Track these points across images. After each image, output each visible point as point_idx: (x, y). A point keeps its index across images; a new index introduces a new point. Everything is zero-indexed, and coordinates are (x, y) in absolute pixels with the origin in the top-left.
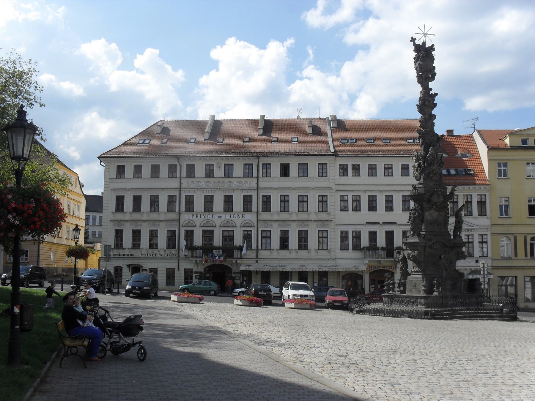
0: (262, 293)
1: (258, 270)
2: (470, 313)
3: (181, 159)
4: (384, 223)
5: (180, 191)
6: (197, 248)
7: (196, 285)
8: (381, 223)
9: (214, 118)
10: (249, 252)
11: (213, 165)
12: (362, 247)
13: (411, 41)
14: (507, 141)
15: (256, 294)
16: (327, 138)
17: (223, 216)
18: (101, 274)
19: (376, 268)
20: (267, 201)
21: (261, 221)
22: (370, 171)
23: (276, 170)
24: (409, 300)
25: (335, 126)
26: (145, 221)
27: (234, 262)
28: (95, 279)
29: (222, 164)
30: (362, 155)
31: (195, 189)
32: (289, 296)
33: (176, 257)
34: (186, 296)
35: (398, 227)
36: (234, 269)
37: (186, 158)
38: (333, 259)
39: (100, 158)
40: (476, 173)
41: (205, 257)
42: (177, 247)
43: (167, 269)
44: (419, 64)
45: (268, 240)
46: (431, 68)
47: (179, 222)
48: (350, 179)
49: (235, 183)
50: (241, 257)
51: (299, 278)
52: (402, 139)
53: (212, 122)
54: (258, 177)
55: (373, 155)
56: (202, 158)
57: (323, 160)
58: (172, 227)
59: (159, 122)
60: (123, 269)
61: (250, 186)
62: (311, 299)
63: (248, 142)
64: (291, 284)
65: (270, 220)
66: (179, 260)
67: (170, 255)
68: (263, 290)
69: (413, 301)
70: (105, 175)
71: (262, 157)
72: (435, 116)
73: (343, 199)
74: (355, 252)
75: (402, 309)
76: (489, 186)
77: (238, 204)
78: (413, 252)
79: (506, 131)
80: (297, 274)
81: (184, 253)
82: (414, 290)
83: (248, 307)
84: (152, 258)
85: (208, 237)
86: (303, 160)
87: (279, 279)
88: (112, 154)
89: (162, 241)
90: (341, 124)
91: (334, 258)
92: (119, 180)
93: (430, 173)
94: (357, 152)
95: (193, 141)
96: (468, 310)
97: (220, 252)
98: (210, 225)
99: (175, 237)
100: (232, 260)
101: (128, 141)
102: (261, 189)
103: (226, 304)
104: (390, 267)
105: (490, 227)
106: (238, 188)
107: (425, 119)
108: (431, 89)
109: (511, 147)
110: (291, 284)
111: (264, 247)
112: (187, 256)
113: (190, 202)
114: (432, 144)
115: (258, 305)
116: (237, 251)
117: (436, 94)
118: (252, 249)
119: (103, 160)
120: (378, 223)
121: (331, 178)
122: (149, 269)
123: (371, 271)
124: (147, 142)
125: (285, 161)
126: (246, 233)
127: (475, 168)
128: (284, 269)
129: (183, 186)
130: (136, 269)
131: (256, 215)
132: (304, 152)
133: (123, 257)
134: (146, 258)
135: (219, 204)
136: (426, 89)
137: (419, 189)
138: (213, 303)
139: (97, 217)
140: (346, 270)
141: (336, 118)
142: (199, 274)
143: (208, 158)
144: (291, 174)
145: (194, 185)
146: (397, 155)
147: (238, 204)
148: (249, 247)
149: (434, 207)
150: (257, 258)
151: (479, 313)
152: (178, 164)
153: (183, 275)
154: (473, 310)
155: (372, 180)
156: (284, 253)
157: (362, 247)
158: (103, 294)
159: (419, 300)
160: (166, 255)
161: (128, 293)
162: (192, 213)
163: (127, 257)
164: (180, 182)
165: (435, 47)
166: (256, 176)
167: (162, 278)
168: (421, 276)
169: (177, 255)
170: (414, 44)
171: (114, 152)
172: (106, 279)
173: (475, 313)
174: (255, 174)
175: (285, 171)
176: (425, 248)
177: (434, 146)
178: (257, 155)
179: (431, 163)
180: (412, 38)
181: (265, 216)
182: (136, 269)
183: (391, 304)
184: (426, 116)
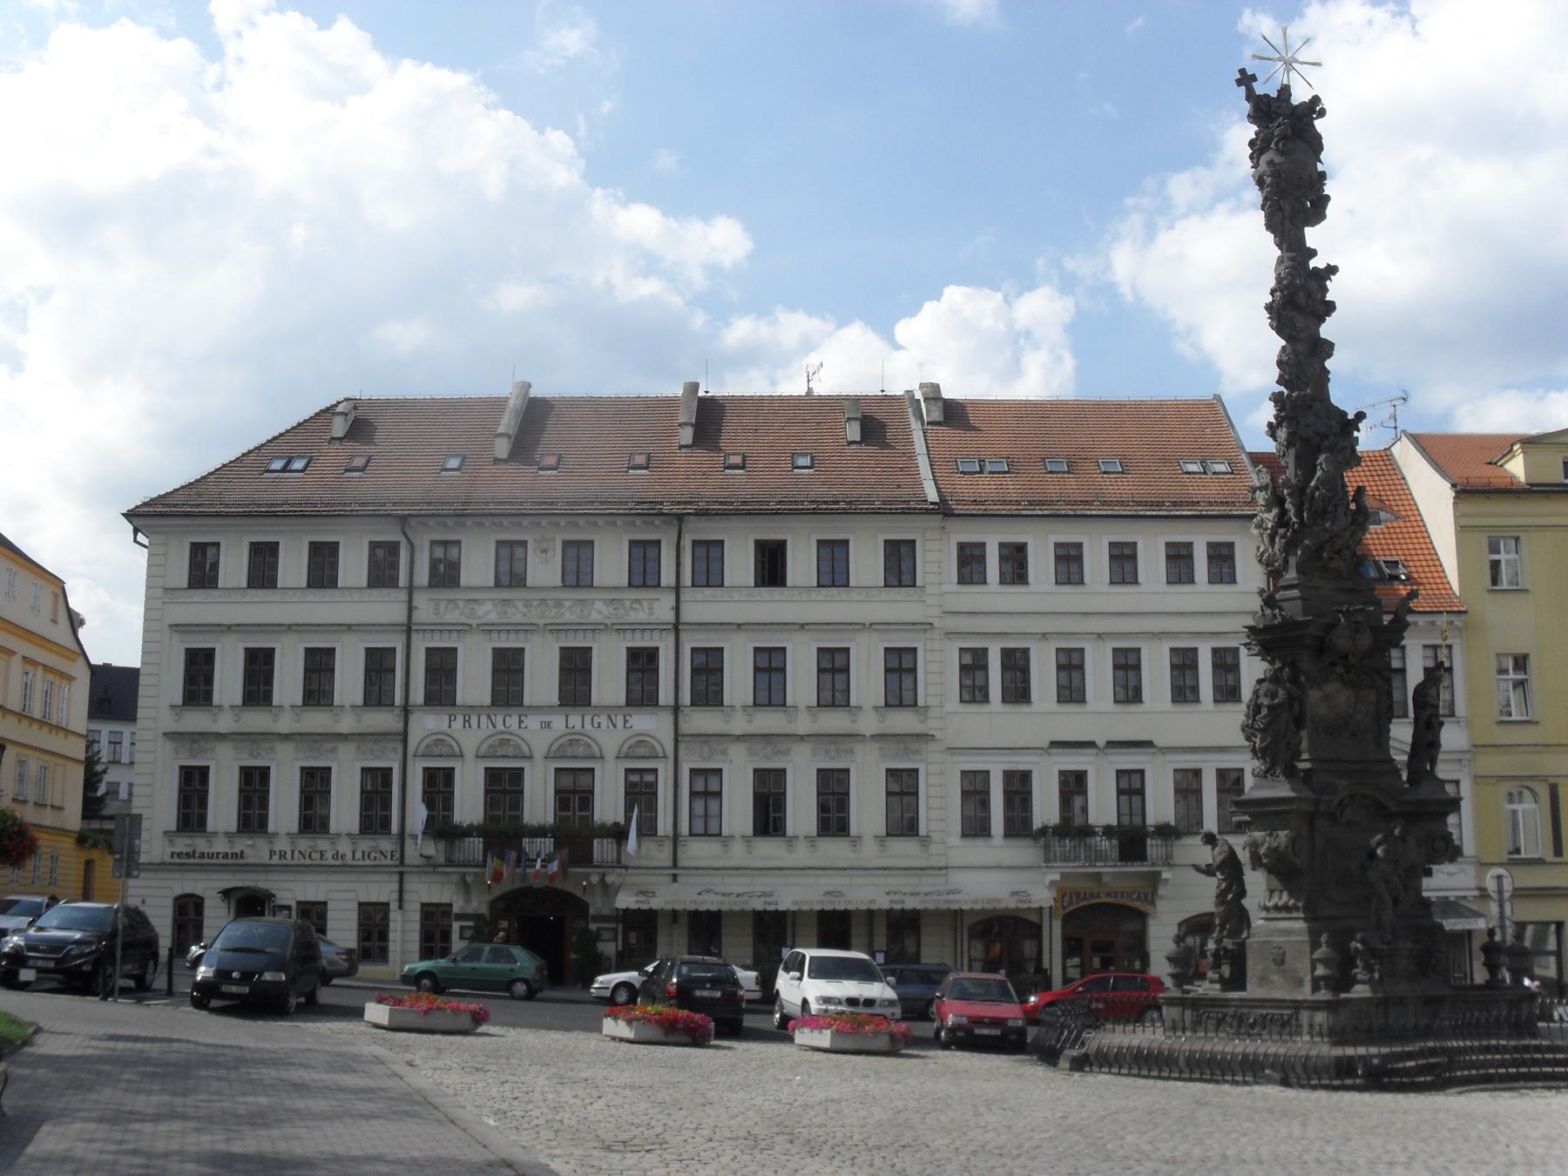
0: (706, 994)
1: (679, 907)
2: (1502, 1064)
3: (413, 522)
4: (1112, 744)
7: (464, 960)
8: (1101, 743)
9: (527, 392)
10: (649, 845)
11: (524, 543)
12: (1037, 823)
13: (1239, 82)
14: (1517, 467)
15: (684, 996)
16: (911, 456)
17: (558, 722)
19: (1085, 898)
20: (708, 668)
22: (1062, 568)
23: (740, 563)
24: (1264, 1017)
25: (937, 419)
26: (286, 737)
27: (595, 879)
28: (78, 942)
29: (554, 540)
30: (1035, 513)
31: (462, 629)
32: (805, 1002)
33: (392, 863)
34: (424, 1005)
35: (1160, 758)
36: (596, 905)
37: (432, 522)
38: (940, 869)
40: (1416, 575)
41: (493, 863)
43: (361, 904)
44: (1271, 163)
45: (713, 804)
46: (1311, 176)
47: (405, 742)
48: (993, 594)
49: (599, 606)
50: (619, 864)
51: (818, 940)
52: (1165, 460)
53: (520, 402)
54: (677, 588)
55: (1072, 513)
57: (900, 530)
59: (339, 403)
60: (207, 903)
61: (652, 619)
62: (888, 1012)
64: (811, 958)
66: (401, 874)
69: (1283, 1019)
71: (692, 517)
72: (1330, 346)
73: (974, 664)
74: (1013, 842)
75: (1239, 1049)
76: (1463, 617)
77: (609, 681)
78: (1271, 835)
79: (1515, 436)
81: (420, 848)
82: (1275, 978)
84: (307, 866)
85: (505, 792)
86: (834, 530)
87: (750, 940)
88: (175, 506)
89: (345, 808)
90: (954, 414)
91: (942, 863)
92: (199, 595)
93: (1320, 548)
95: (806, 461)
96: (1487, 1050)
97: (547, 845)
98: (510, 751)
99: (391, 793)
100: (589, 874)
101: (231, 462)
102: (688, 627)
103: (573, 1035)
104: (1133, 893)
105: (1468, 756)
106: (608, 622)
107: (1296, 357)
108: (1313, 253)
109: (1532, 485)
110: (811, 958)
111: (699, 828)
113: (442, 668)
114: (1326, 443)
115: (696, 1038)
116: (605, 841)
117: (1332, 270)
118: (656, 834)
120: (1091, 744)
121: (930, 589)
122: (299, 903)
123: (1068, 910)
124: (298, 465)
125: (771, 531)
126: (635, 778)
127: (1409, 558)
129: (417, 618)
130: (250, 903)
132: (837, 502)
134: (287, 866)
135: (542, 679)
136: (1295, 252)
137: (1284, 605)
138: (524, 1031)
140: (987, 906)
141: (939, 391)
142: (471, 924)
143: (506, 522)
144: (791, 577)
145: (457, 612)
146: (1154, 513)
147: (609, 681)
148: (648, 829)
149: (1340, 670)
150: (675, 865)
151: (1535, 1063)
153: (416, 926)
154: (1505, 1049)
155: (1069, 598)
156: (769, 850)
157: (1037, 823)
158: (104, 999)
159: (1304, 1016)
160: (359, 855)
161: (205, 997)
163: (221, 861)
164: (410, 601)
165: (1326, 103)
166: (673, 582)
167: (342, 932)
168: (1301, 925)
169: (398, 855)
170: (1251, 95)
171: (179, 499)
173: (1514, 1063)
174: (667, 577)
175: (771, 564)
176: (1312, 818)
177: (1331, 450)
178: (676, 509)
179: (1325, 512)
180: (1242, 71)
181: (701, 721)
182: (250, 903)
183: (1194, 1031)
184: (1300, 347)
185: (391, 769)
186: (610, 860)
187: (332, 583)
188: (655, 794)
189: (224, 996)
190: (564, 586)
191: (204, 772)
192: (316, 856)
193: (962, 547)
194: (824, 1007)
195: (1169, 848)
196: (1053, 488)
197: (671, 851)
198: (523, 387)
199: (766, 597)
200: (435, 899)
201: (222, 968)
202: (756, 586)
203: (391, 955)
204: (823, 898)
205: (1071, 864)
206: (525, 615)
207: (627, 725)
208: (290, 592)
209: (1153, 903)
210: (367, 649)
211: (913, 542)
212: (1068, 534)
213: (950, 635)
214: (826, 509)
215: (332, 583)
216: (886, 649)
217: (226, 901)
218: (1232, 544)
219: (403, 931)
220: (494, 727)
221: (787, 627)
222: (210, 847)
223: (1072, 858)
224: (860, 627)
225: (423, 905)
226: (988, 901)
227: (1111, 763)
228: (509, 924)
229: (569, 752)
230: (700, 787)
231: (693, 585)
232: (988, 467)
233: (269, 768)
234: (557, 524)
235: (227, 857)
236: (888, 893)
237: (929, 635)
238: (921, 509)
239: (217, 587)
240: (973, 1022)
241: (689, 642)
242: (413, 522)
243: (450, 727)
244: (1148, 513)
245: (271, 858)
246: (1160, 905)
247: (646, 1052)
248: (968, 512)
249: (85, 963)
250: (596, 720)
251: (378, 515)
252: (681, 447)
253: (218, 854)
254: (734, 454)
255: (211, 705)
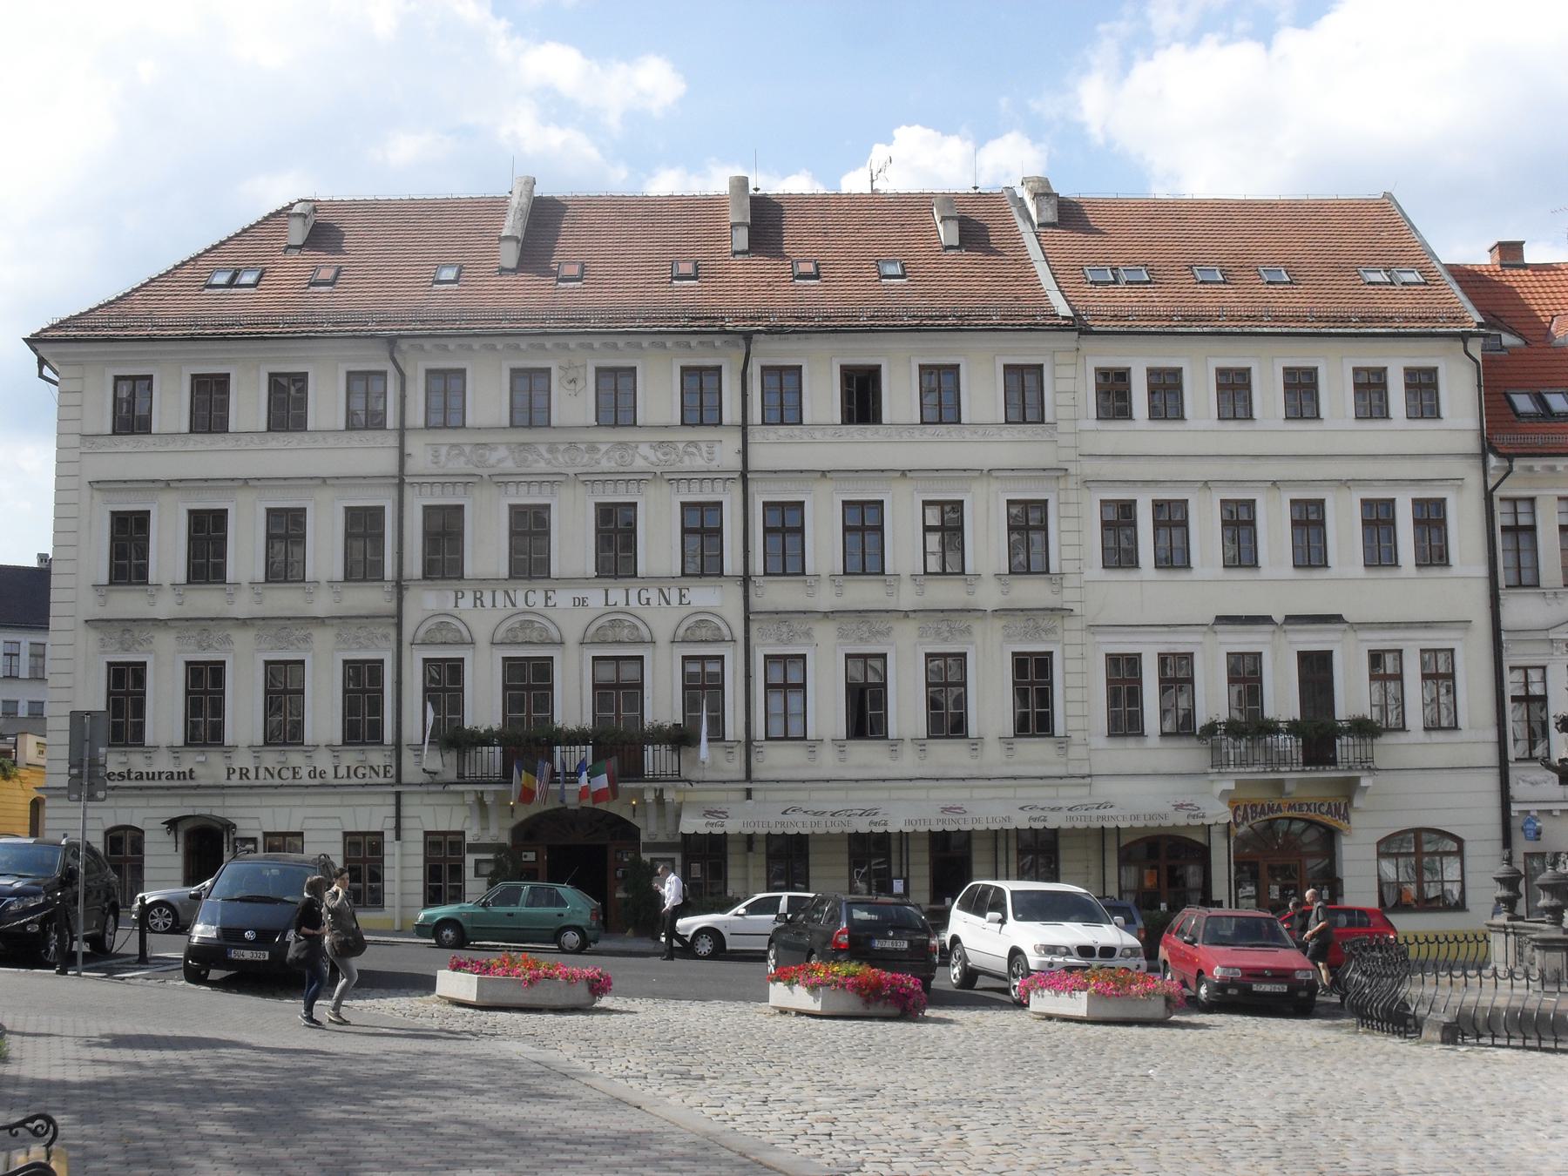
0: (888, 944)
4: (1291, 619)
5: (401, 485)
6: (485, 739)
8: (1278, 617)
12: (1201, 720)
16: (1026, 263)
17: (595, 598)
18: (53, 866)
19: (1263, 812)
21: (761, 617)
25: (1050, 220)
26: (244, 623)
27: (650, 797)
28: (18, 894)
29: (585, 366)
30: (1192, 330)
35: (1351, 636)
36: (650, 829)
37: (428, 344)
39: (37, 346)
41: (520, 778)
42: (388, 735)
43: (346, 834)
47: (399, 626)
49: (644, 450)
52: (1339, 268)
53: (525, 200)
54: (744, 427)
55: (1238, 330)
56: (499, 344)
57: (1025, 351)
58: (367, 648)
60: (147, 837)
61: (713, 466)
62: (1131, 963)
63: (695, 278)
65: (805, 612)
66: (398, 795)
67: (360, 771)
68: (892, 928)
70: (57, 490)
73: (1120, 518)
80: (925, 844)
83: (856, 1024)
84: (276, 787)
86: (940, 351)
91: (1086, 771)
92: (128, 443)
94: (1170, 318)
95: (449, 274)
98: (535, 637)
99: (382, 692)
100: (642, 791)
101: (161, 276)
104: (1322, 804)
106: (658, 470)
111: (777, 730)
112: (435, 773)
118: (723, 739)
119: (55, 355)
120: (1266, 620)
121: (1062, 426)
122: (266, 834)
125: (861, 353)
126: (694, 668)
128: (876, 824)
129: (412, 466)
131: (739, 591)
133: (145, 783)
134: (252, 787)
139: (20, 705)
140: (1152, 824)
141: (1049, 187)
142: (490, 856)
143: (523, 343)
145: (463, 459)
146: (1340, 330)
148: (717, 734)
150: (748, 778)
152: (390, 368)
153: (420, 861)
155: (1236, 436)
156: (866, 754)
157: (1201, 720)
158: (63, 972)
160: (342, 771)
162: (456, 584)
163: (164, 782)
164: (402, 447)
169: (393, 771)
172: (81, 889)
174: (731, 412)
178: (741, 326)
181: (777, 594)
185: (382, 661)
186: (479, 774)
187: (300, 425)
188: (722, 687)
189: (230, 964)
190: (598, 425)
191: (139, 670)
192: (287, 774)
193: (1103, 373)
194: (1048, 959)
195: (1369, 748)
196: (1208, 301)
197: (743, 757)
198: (526, 183)
199: (857, 437)
200: (443, 826)
201: (227, 926)
202: (843, 423)
203: (387, 900)
204: (942, 816)
205: (1248, 770)
206: (549, 463)
207: (550, 603)
208: (247, 437)
209: (1346, 818)
210: (348, 509)
211: (1040, 367)
212: (1233, 356)
213: (1087, 483)
214: (932, 325)
215: (300, 425)
216: (845, 503)
217: (173, 833)
218: (1435, 370)
219: (402, 868)
220: (514, 605)
221: (885, 474)
222: (150, 765)
223: (1250, 761)
224: (977, 474)
225: (427, 834)
226: (1151, 817)
227: (1291, 643)
228: (537, 857)
229: (610, 636)
230: (777, 678)
231: (764, 423)
232: (1124, 277)
233: (223, 663)
234: (590, 347)
235: (172, 778)
236: (1022, 808)
237: (1062, 484)
238: (1051, 325)
239: (306, 430)
240: (1249, 975)
241: (761, 495)
242: (404, 345)
243: (456, 606)
244: (1332, 330)
245: (229, 778)
246: (1354, 817)
247: (1067, 1029)
248: (1109, 329)
249: (31, 922)
250: (644, 595)
251: (359, 337)
252: (735, 253)
253: (160, 773)
254: (805, 261)
255: (147, 583)
